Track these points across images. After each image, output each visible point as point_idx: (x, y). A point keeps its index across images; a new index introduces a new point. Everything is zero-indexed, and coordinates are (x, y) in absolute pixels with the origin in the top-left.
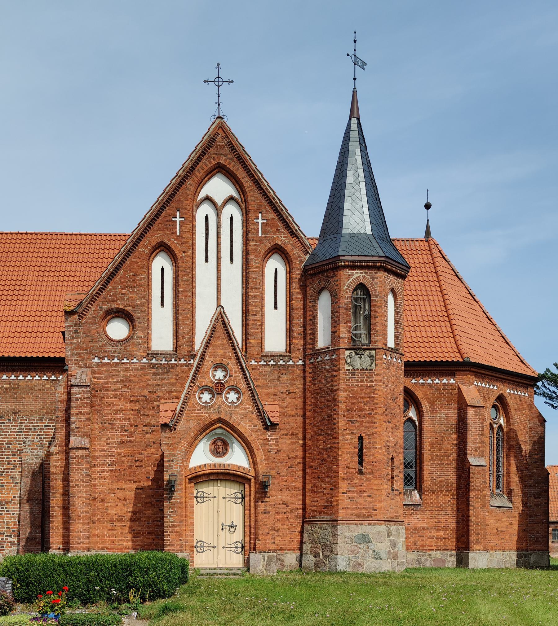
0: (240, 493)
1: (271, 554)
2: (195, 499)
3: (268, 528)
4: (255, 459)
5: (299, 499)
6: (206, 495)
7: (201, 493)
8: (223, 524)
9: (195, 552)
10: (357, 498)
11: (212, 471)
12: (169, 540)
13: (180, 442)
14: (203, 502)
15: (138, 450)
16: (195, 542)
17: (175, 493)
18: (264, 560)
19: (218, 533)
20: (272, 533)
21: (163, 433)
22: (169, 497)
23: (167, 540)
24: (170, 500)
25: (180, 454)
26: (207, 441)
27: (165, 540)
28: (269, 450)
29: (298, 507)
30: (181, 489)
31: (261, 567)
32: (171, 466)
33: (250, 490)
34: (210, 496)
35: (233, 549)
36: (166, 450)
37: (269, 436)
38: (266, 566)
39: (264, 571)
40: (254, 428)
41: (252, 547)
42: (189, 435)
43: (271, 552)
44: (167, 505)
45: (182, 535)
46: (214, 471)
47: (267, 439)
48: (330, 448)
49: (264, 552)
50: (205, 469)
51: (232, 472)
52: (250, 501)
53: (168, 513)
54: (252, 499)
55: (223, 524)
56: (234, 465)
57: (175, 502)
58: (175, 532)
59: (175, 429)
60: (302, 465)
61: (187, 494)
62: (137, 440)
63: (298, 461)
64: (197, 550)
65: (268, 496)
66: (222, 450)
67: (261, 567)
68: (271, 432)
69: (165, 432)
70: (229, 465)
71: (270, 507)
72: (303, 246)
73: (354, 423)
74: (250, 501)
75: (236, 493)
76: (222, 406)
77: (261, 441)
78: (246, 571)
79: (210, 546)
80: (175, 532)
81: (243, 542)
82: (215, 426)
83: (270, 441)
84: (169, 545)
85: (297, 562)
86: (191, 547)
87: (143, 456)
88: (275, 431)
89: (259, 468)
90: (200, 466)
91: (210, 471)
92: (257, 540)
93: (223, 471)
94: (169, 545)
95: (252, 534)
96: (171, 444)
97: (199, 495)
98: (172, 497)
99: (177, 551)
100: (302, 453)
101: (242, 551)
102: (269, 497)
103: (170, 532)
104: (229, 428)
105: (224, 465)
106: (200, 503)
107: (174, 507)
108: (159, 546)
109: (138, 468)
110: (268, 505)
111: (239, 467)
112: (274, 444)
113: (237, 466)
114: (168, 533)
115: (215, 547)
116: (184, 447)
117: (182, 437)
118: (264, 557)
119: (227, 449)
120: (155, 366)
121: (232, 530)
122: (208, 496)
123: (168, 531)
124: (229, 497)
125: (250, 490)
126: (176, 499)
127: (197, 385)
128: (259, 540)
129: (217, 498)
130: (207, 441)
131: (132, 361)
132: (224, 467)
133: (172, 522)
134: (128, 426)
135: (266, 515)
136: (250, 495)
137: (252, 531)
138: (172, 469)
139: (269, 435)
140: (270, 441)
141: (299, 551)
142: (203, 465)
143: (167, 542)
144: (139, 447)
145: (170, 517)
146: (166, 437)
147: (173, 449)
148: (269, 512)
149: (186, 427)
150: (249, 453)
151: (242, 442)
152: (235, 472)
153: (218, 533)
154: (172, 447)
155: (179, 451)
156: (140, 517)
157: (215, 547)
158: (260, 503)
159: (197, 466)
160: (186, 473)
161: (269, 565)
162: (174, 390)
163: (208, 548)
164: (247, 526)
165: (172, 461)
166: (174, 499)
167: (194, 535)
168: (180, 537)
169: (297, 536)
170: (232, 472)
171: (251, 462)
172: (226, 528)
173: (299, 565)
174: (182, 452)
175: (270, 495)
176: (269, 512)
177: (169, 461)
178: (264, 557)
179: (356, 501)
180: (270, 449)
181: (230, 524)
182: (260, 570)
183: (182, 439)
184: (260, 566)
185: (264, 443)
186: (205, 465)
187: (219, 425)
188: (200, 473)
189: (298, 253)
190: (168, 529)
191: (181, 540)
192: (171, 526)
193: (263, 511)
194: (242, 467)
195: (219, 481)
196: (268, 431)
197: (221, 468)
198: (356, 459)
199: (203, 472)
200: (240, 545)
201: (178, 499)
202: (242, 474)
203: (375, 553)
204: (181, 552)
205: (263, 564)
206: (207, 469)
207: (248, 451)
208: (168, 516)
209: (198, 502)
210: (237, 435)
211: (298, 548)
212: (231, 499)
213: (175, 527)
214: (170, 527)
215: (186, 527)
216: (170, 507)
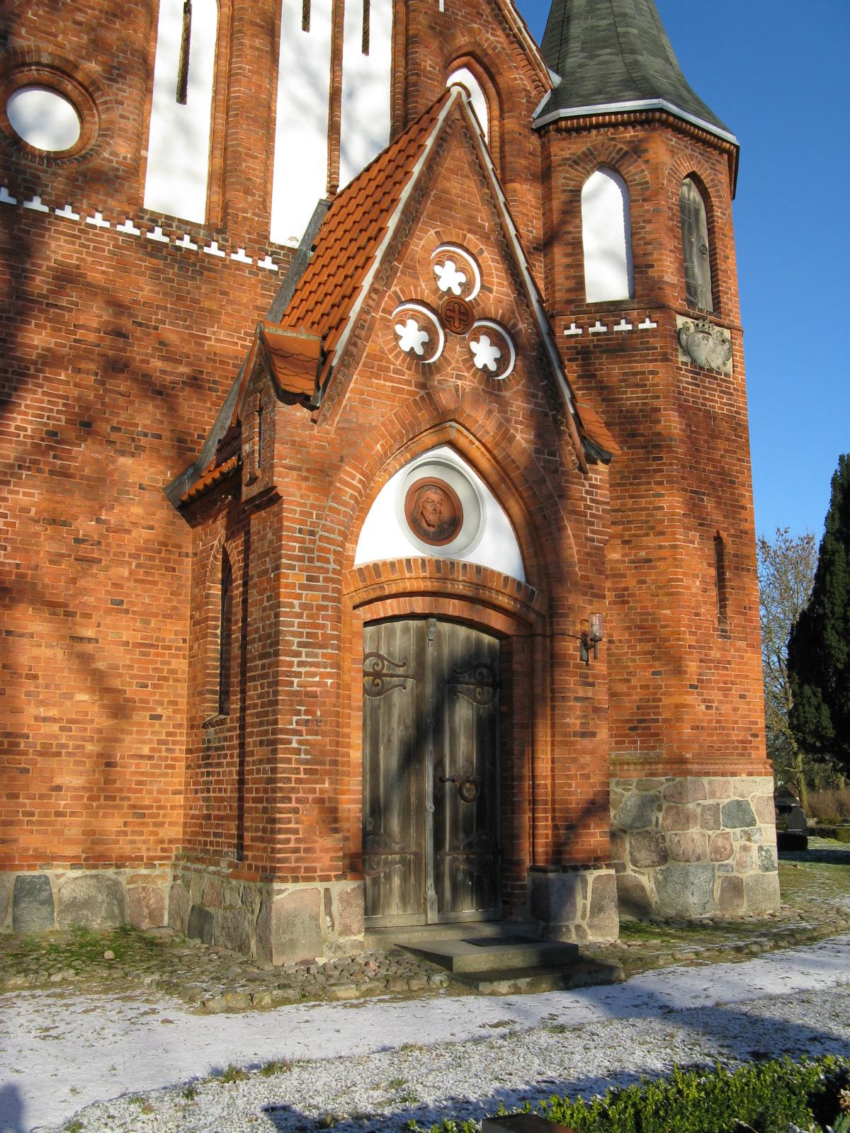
10: (721, 702)
12: (296, 831)
36: (292, 490)
48: (648, 561)
53: (294, 726)
72: (534, 69)
73: (703, 500)
76: (466, 374)
83: (590, 508)
84: (296, 850)
87: (103, 528)
103: (299, 801)
108: (144, 847)
114: (294, 805)
120: (161, 251)
123: (293, 796)
127: (395, 292)
131: (89, 220)
134: (59, 420)
142: (400, 561)
143: (288, 841)
156: (84, 739)
162: (214, 333)
179: (717, 709)
189: (521, 79)
192: (302, 776)
193: (578, 729)
198: (713, 593)
203: (763, 853)
208: (295, 738)
214: (298, 781)
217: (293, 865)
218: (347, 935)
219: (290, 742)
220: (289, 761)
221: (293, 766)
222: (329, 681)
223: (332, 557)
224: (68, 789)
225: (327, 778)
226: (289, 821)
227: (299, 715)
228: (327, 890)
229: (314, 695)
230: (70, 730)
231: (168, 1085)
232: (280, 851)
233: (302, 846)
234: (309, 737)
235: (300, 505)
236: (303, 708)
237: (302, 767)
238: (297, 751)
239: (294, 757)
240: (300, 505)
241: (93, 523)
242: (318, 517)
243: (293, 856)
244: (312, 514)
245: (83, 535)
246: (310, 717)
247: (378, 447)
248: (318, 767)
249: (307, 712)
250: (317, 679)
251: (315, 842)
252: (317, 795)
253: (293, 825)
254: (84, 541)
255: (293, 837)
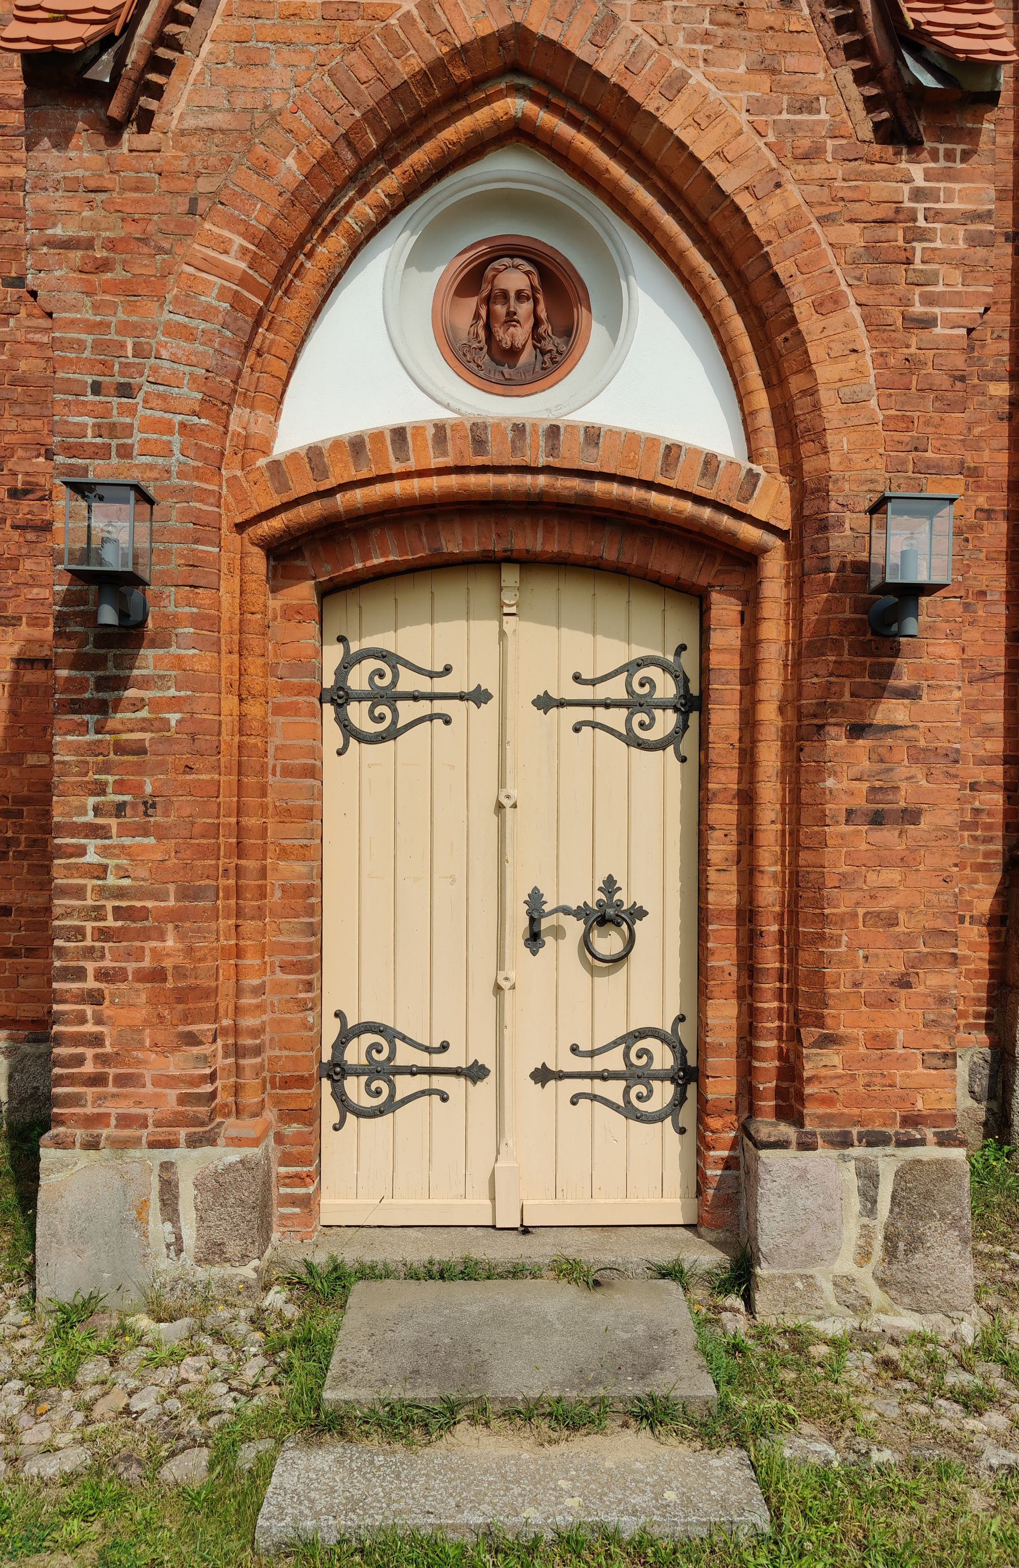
0: (665, 668)
1: (930, 1152)
2: (329, 709)
3: (904, 943)
4: (796, 383)
5: (987, 731)
6: (409, 681)
7: (371, 664)
8: (535, 900)
9: (330, 1111)
11: (453, 481)
12: (97, 1040)
13: (186, 233)
14: (392, 734)
15: (27, 425)
16: (331, 1031)
17: (148, 655)
18: (869, 1200)
19: (500, 965)
20: (933, 981)
21: (47, 155)
22: (101, 684)
23: (78, 1040)
24: (102, 708)
25: (190, 335)
26: (418, 259)
27: (59, 1040)
28: (918, 309)
29: (980, 774)
30: (195, 621)
31: (845, 1264)
32: (113, 430)
33: (751, 644)
34: (441, 685)
35: (613, 1090)
36: (70, 297)
37: (918, 194)
38: (891, 1251)
39: (877, 1296)
40: (793, 128)
41: (767, 1085)
42: (264, 170)
43: (929, 1133)
44: (76, 749)
45: (210, 993)
46: (473, 480)
47: (899, 215)
49: (875, 1140)
50: (396, 467)
51: (615, 489)
52: (749, 722)
53: (90, 817)
54: (769, 713)
55: (535, 900)
56: (632, 438)
57: (145, 726)
58: (143, 976)
59: (145, 122)
60: (1003, 526)
61: (254, 665)
62: (23, 365)
63: (982, 501)
64: (341, 1098)
65: (905, 681)
66: (536, 335)
67: (845, 1264)
68: (934, 157)
69: (62, 141)
70: (593, 435)
71: (918, 771)
74: (749, 722)
75: (641, 663)
77: (854, 235)
78: (724, 1288)
79: (440, 1061)
80: (143, 976)
81: (687, 1035)
82: (482, 117)
83: (922, 235)
84: (97, 1080)
85: (971, 1103)
86: (287, 1083)
88: (966, 156)
89: (834, 460)
90: (357, 445)
91: (435, 484)
92: (809, 1034)
93: (542, 480)
94: (97, 1080)
95: (769, 986)
96: (111, 245)
97: (358, 679)
98: (122, 683)
99: (163, 1133)
100: (1004, 457)
101: (680, 1100)
102: (910, 694)
103: (102, 975)
104: (591, 134)
105: (554, 431)
106: (363, 738)
107: (140, 769)
109: (31, 536)
110: (901, 754)
111: (672, 452)
112: (961, 263)
113: (652, 441)
114: (91, 984)
115: (475, 1073)
116: (226, 272)
117: (204, 185)
118: (869, 1178)
119: (568, 331)
121: (610, 943)
122: (423, 684)
123: (90, 967)
124: (585, 693)
125: (751, 644)
126: (156, 705)
128: (828, 1041)
129: (491, 707)
130: (418, 259)
132: (553, 450)
133: (120, 893)
135: (887, 835)
136: (750, 676)
137: (770, 959)
138: (125, 452)
139: (920, 182)
140: (922, 235)
141: (983, 1036)
142: (377, 436)
143: (80, 1060)
144: (29, 409)
145: (104, 852)
146: (73, 186)
147: (129, 291)
148: (911, 816)
149: (241, 101)
150: (745, 343)
151: (696, 257)
152: (634, 493)
153: (500, 965)
154: (118, 274)
155: (185, 302)
157: (475, 1073)
158: (836, 740)
159: (336, 444)
160: (242, 498)
161: (916, 1242)
163: (421, 1082)
164: (720, 915)
165: (125, 390)
166: (138, 705)
167: (309, 986)
168: (186, 1018)
169: (973, 946)
170: (615, 489)
171: (765, 419)
172: (558, 932)
173: (982, 1116)
174: (207, 314)
175: (925, 673)
176: (911, 816)
177: (97, 388)
178: (869, 1178)
180: (929, 300)
181: (588, 895)
182: (843, 1284)
183: (203, 205)
184: (835, 1252)
185: (873, 253)
186: (399, 433)
187: (517, 105)
188: (359, 496)
190: (89, 953)
191: (192, 1039)
192: (110, 922)
193: (860, 802)
194: (695, 451)
195: (510, 576)
196: (913, 145)
197: (527, 460)
199: (378, 492)
200: (663, 1058)
201: (174, 703)
202: (688, 507)
204: (193, 1142)
205: (866, 1233)
206: (412, 465)
207: (737, 324)
208: (92, 845)
209: (349, 731)
210: (653, 189)
211: (977, 1015)
212: (602, 715)
213: (145, 935)
214: (104, 934)
215: (249, 926)
216: (106, 768)
217: (89, 1110)
218: (211, 1263)
219: (82, 851)
220: (79, 892)
221: (89, 902)
222: (174, 718)
223: (176, 441)
224: (21, 911)
225: (170, 926)
226: (82, 1020)
227: (103, 793)
228: (167, 1166)
229: (140, 750)
230: (20, 814)
231: (529, 1281)
232: (60, 1080)
233: (112, 1072)
234: (127, 841)
235: (91, 327)
236: (110, 779)
237: (109, 905)
238: (101, 872)
239: (90, 883)
240: (91, 327)
241: (42, 459)
242: (139, 351)
243: (90, 1092)
244: (122, 346)
245: (24, 483)
246: (127, 798)
247: (290, 161)
248: (149, 904)
249: (121, 787)
250: (144, 713)
251: (139, 1062)
252: (147, 963)
253: (89, 1028)
254: (26, 492)
255: (89, 1052)
